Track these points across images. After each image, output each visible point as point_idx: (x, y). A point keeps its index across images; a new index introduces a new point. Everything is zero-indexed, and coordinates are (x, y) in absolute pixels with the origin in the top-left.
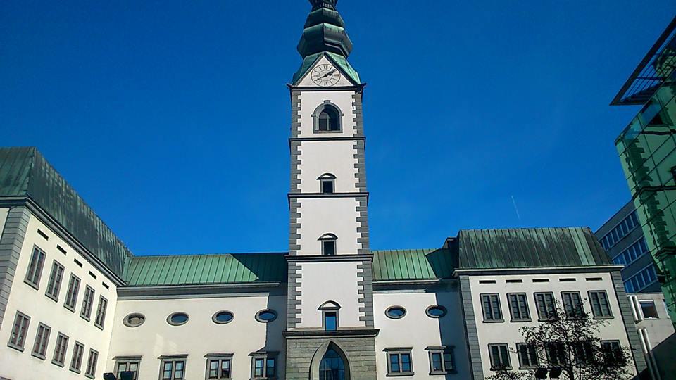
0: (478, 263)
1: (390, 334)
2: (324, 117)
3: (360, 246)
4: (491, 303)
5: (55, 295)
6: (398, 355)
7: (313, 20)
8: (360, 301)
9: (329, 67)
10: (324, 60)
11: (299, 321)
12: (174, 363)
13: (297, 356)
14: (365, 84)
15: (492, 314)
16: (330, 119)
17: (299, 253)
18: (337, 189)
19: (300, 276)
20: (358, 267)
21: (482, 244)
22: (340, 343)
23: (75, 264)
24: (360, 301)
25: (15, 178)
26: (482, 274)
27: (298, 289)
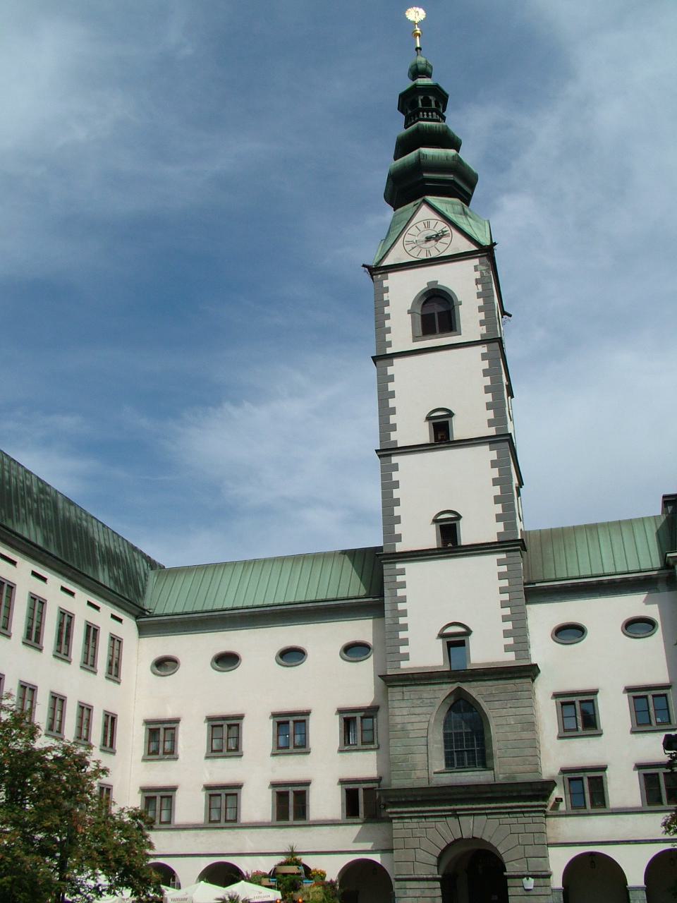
1: (560, 669)
2: (428, 311)
5: (38, 640)
6: (646, 697)
7: (404, 146)
8: (505, 619)
9: (432, 223)
10: (424, 212)
11: (406, 657)
13: (405, 712)
14: (510, 316)
19: (403, 585)
20: (500, 563)
22: (474, 690)
24: (505, 619)
27: (401, 606)
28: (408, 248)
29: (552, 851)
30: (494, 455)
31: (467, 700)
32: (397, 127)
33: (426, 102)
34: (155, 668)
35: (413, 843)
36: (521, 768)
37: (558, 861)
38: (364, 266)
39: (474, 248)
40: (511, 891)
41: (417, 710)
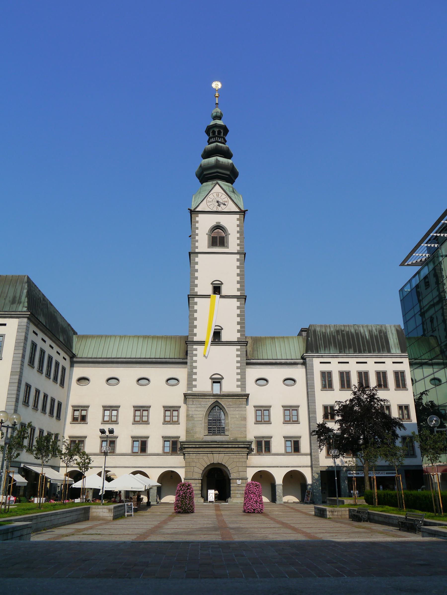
0: (320, 349)
3: (239, 335)
4: (326, 377)
9: (220, 195)
11: (195, 386)
12: (142, 411)
13: (193, 409)
14: (247, 210)
15: (327, 383)
16: (218, 238)
17: (196, 339)
18: (224, 293)
20: (238, 350)
21: (324, 335)
22: (223, 402)
23: (42, 341)
25: (18, 298)
26: (322, 357)
27: (194, 364)
28: (209, 204)
29: (249, 469)
30: (238, 304)
31: (217, 408)
32: (203, 143)
33: (219, 132)
34: (78, 383)
35: (193, 464)
36: (239, 436)
37: (250, 473)
38: (189, 209)
39: (237, 210)
40: (232, 485)
41: (199, 409)
